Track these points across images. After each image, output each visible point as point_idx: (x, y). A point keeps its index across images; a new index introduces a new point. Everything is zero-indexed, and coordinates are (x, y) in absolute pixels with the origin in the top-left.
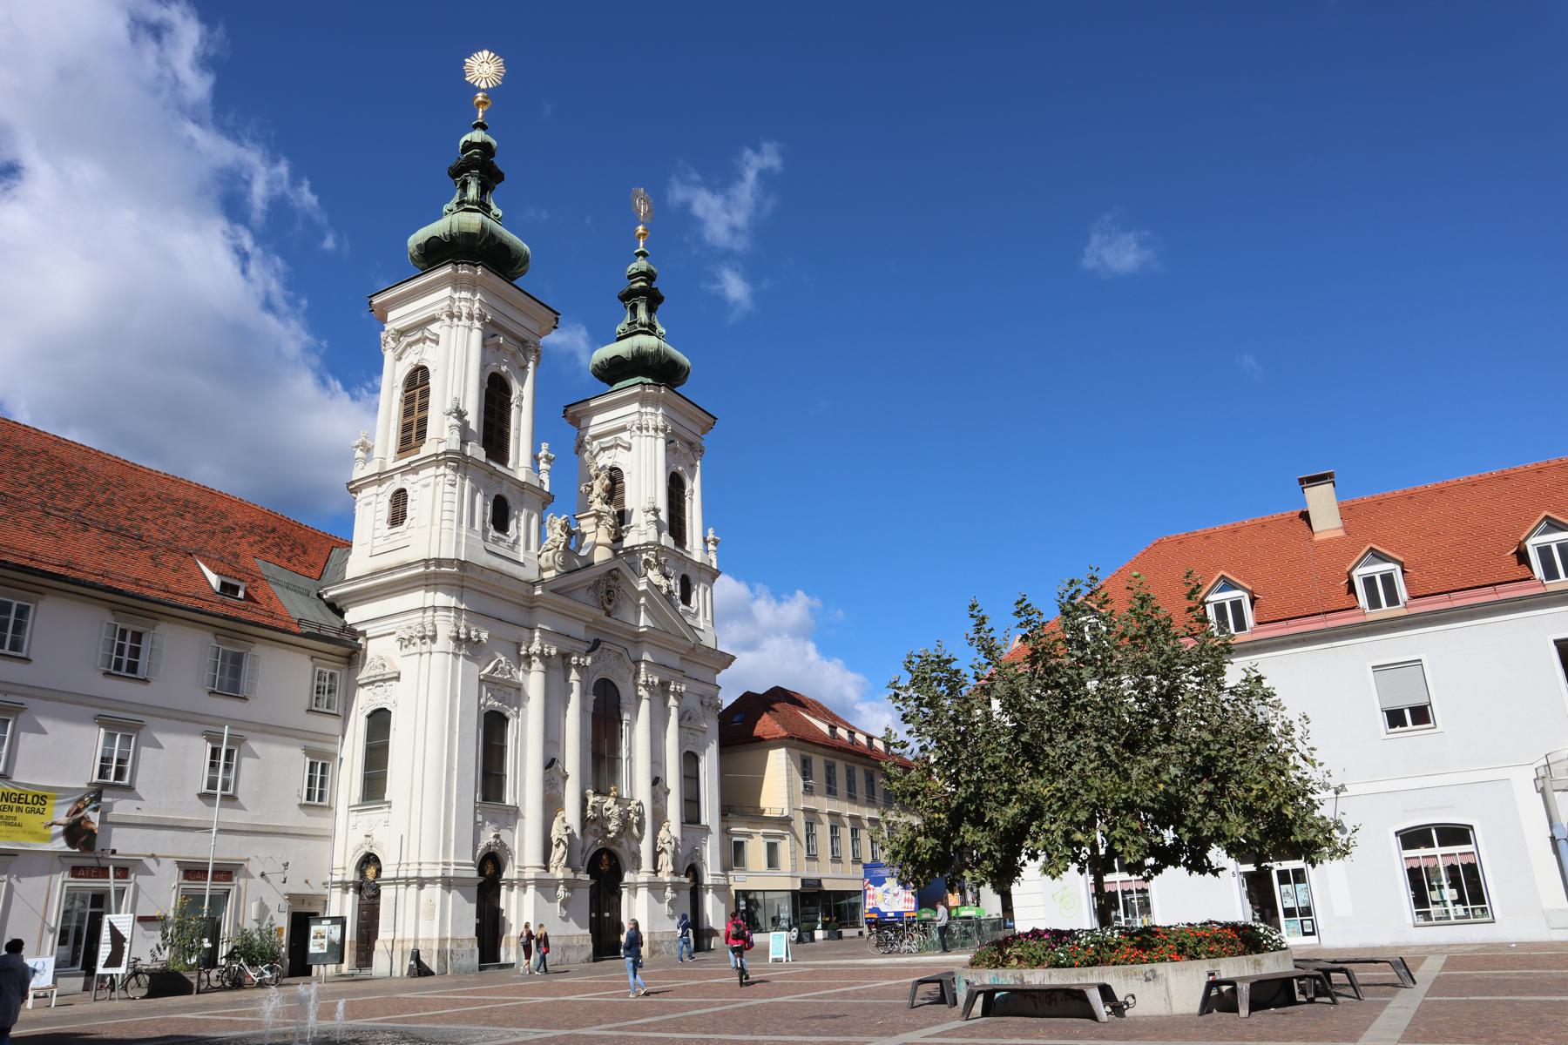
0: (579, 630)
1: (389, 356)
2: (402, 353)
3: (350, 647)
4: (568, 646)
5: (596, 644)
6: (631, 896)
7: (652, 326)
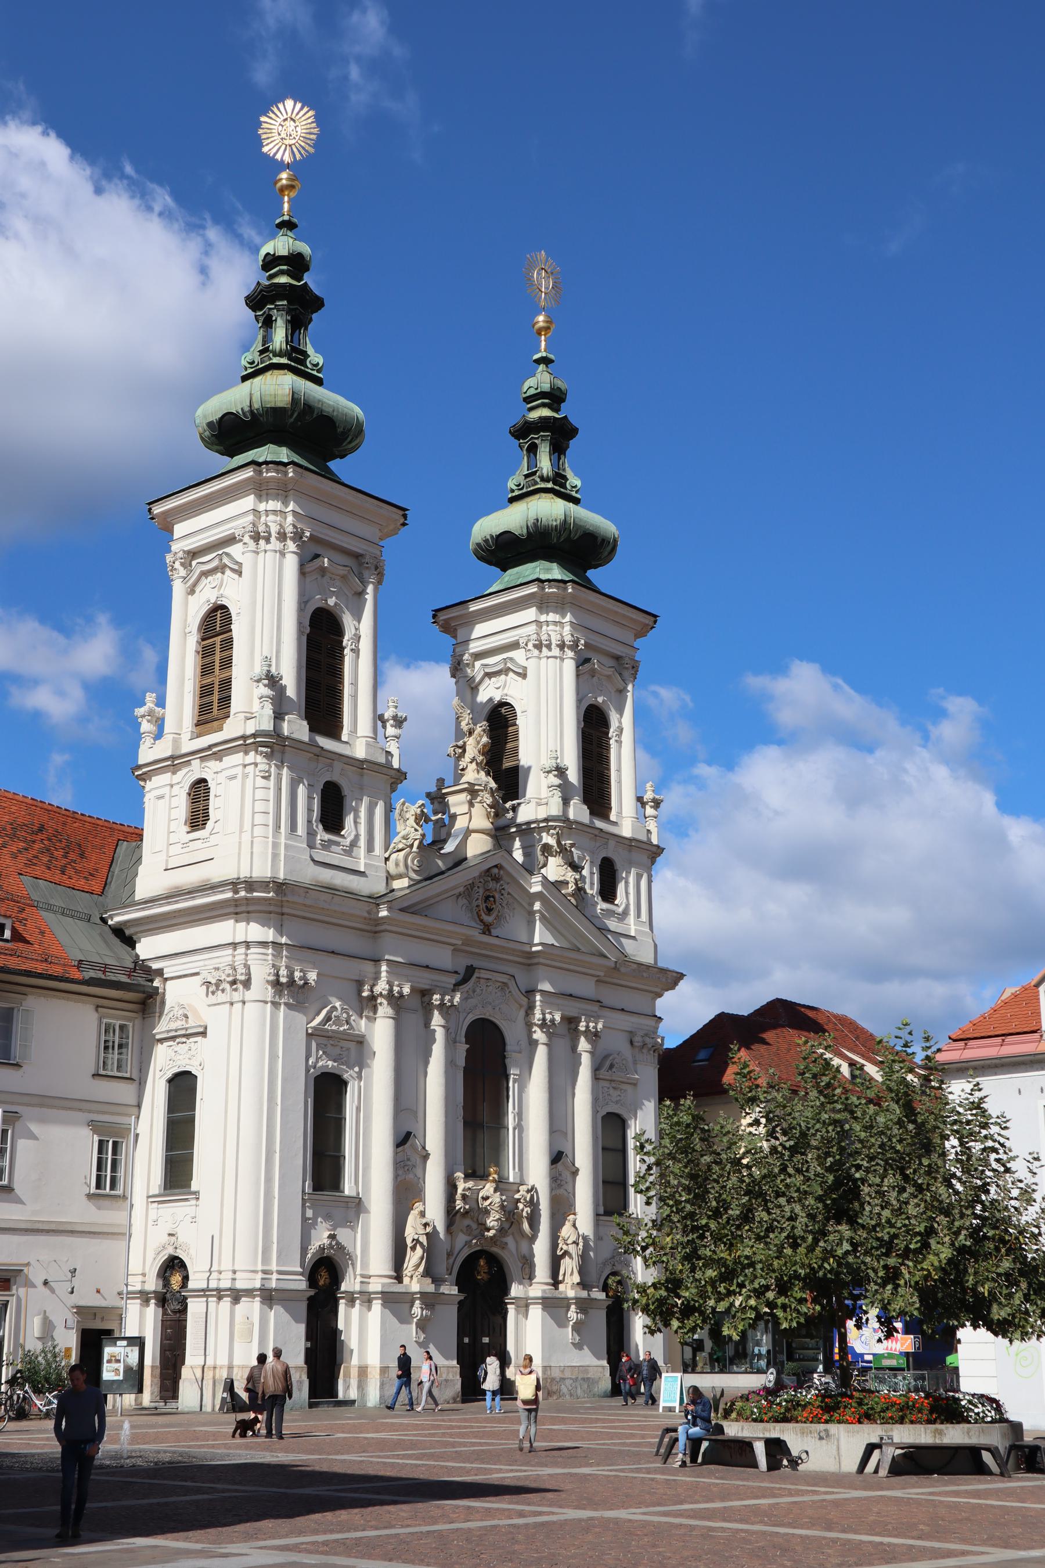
0: (443, 958)
1: (178, 588)
2: (195, 584)
3: (144, 992)
4: (425, 979)
5: (470, 971)
6: (520, 1316)
7: (559, 478)
